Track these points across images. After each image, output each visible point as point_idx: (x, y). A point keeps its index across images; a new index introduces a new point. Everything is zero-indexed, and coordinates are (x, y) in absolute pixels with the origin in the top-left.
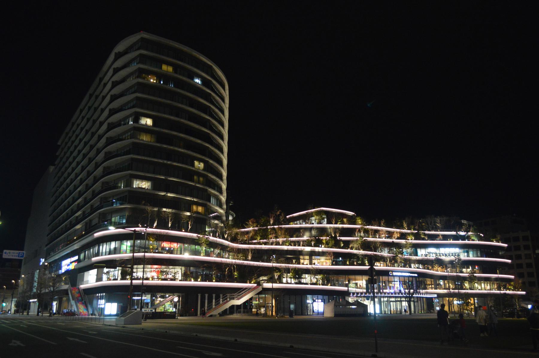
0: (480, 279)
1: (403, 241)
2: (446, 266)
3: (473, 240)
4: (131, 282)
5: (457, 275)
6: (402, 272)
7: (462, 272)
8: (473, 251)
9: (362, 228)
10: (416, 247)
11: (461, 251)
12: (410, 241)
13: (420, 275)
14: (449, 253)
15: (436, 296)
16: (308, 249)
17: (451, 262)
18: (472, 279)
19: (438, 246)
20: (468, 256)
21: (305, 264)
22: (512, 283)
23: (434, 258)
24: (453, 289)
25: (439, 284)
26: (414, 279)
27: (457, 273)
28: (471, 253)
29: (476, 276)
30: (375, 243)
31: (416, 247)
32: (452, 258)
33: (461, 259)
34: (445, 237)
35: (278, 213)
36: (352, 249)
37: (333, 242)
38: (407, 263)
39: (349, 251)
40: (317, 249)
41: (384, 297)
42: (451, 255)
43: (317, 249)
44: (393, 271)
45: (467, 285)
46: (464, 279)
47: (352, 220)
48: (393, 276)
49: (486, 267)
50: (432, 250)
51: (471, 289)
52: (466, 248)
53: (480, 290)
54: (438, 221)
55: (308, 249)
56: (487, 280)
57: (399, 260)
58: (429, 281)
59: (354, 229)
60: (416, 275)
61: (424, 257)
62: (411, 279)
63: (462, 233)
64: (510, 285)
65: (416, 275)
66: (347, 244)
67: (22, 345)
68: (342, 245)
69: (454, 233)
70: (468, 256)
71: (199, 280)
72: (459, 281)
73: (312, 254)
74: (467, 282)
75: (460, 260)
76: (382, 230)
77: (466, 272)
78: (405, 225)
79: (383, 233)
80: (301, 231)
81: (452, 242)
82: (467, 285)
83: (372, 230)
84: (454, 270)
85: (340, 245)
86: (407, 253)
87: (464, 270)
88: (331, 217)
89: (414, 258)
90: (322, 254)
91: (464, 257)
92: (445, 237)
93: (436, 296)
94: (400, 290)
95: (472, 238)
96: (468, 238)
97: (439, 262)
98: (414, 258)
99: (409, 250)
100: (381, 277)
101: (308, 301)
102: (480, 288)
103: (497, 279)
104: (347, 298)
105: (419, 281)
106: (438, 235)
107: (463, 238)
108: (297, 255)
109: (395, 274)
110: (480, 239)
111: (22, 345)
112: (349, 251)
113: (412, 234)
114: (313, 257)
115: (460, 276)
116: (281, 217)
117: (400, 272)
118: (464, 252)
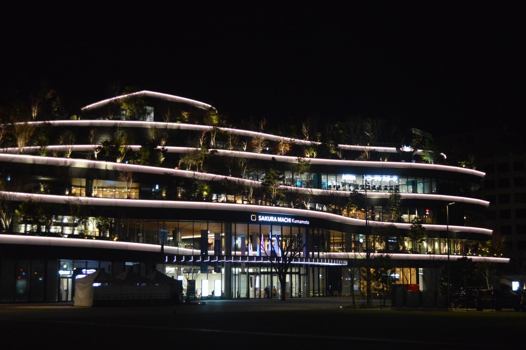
0: (432, 235)
1: (293, 159)
2: (373, 209)
3: (427, 162)
4: (162, 248)
5: (390, 226)
6: (277, 216)
7: (401, 221)
8: (424, 183)
9: (213, 131)
10: (319, 171)
11: (403, 181)
12: (307, 159)
13: (315, 221)
14: (381, 184)
15: (346, 263)
16: (81, 163)
17: (383, 202)
18: (417, 234)
19: (360, 171)
20: (415, 191)
21: (78, 196)
22: (488, 243)
23: (348, 192)
24: (380, 251)
25: (357, 243)
26: (303, 230)
27: (392, 221)
28: (420, 187)
29: (424, 228)
30: (236, 159)
31: (319, 171)
32: (386, 194)
33: (400, 196)
34: (375, 156)
35: (49, 96)
36: (183, 167)
37: (148, 153)
38: (294, 198)
39: (176, 171)
40: (105, 165)
41: (236, 265)
42: (388, 188)
43: (105, 165)
44: (258, 213)
45: (408, 245)
46: (402, 233)
47: (198, 116)
48: (258, 222)
49: (438, 211)
50: (349, 178)
51: (413, 251)
52: (412, 176)
53: (430, 253)
54: (369, 126)
55: (81, 163)
56: (444, 235)
57: (274, 193)
58: (336, 237)
59: (198, 133)
60: (307, 222)
61: (333, 191)
62: (295, 230)
63: (407, 149)
64: (484, 246)
65: (307, 222)
66: (172, 160)
67: (184, 293)
68: (162, 159)
69: (393, 149)
70: (415, 191)
71: (115, 240)
72: (393, 237)
73: (92, 175)
74: (407, 239)
75: (397, 197)
76: (258, 138)
77: (407, 221)
78: (305, 130)
79: (258, 144)
80: (92, 132)
81: (386, 163)
82: (408, 245)
83: (234, 135)
84: (388, 216)
85: (158, 158)
86: (299, 183)
87: (405, 216)
88: (163, 110)
89: (316, 191)
90: (114, 175)
91: (406, 192)
92: (375, 156)
93: (346, 263)
94: (273, 252)
95: (425, 158)
96: (419, 159)
97: (358, 201)
98: (316, 191)
99: (304, 177)
100: (233, 225)
101: (61, 272)
102: (430, 250)
103: (462, 235)
104: (159, 267)
105: (315, 235)
106: (362, 152)
107: (408, 157)
108: (61, 179)
109: (261, 218)
110: (439, 160)
111: (184, 293)
112: (176, 171)
113: (314, 146)
114: (95, 183)
115: (395, 227)
116: (54, 104)
117: (276, 215)
118: (408, 184)
